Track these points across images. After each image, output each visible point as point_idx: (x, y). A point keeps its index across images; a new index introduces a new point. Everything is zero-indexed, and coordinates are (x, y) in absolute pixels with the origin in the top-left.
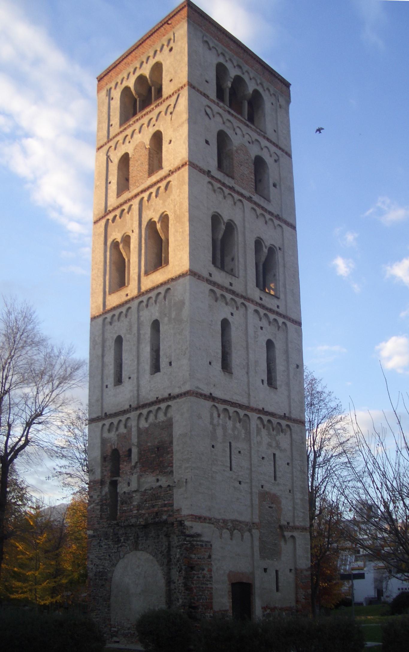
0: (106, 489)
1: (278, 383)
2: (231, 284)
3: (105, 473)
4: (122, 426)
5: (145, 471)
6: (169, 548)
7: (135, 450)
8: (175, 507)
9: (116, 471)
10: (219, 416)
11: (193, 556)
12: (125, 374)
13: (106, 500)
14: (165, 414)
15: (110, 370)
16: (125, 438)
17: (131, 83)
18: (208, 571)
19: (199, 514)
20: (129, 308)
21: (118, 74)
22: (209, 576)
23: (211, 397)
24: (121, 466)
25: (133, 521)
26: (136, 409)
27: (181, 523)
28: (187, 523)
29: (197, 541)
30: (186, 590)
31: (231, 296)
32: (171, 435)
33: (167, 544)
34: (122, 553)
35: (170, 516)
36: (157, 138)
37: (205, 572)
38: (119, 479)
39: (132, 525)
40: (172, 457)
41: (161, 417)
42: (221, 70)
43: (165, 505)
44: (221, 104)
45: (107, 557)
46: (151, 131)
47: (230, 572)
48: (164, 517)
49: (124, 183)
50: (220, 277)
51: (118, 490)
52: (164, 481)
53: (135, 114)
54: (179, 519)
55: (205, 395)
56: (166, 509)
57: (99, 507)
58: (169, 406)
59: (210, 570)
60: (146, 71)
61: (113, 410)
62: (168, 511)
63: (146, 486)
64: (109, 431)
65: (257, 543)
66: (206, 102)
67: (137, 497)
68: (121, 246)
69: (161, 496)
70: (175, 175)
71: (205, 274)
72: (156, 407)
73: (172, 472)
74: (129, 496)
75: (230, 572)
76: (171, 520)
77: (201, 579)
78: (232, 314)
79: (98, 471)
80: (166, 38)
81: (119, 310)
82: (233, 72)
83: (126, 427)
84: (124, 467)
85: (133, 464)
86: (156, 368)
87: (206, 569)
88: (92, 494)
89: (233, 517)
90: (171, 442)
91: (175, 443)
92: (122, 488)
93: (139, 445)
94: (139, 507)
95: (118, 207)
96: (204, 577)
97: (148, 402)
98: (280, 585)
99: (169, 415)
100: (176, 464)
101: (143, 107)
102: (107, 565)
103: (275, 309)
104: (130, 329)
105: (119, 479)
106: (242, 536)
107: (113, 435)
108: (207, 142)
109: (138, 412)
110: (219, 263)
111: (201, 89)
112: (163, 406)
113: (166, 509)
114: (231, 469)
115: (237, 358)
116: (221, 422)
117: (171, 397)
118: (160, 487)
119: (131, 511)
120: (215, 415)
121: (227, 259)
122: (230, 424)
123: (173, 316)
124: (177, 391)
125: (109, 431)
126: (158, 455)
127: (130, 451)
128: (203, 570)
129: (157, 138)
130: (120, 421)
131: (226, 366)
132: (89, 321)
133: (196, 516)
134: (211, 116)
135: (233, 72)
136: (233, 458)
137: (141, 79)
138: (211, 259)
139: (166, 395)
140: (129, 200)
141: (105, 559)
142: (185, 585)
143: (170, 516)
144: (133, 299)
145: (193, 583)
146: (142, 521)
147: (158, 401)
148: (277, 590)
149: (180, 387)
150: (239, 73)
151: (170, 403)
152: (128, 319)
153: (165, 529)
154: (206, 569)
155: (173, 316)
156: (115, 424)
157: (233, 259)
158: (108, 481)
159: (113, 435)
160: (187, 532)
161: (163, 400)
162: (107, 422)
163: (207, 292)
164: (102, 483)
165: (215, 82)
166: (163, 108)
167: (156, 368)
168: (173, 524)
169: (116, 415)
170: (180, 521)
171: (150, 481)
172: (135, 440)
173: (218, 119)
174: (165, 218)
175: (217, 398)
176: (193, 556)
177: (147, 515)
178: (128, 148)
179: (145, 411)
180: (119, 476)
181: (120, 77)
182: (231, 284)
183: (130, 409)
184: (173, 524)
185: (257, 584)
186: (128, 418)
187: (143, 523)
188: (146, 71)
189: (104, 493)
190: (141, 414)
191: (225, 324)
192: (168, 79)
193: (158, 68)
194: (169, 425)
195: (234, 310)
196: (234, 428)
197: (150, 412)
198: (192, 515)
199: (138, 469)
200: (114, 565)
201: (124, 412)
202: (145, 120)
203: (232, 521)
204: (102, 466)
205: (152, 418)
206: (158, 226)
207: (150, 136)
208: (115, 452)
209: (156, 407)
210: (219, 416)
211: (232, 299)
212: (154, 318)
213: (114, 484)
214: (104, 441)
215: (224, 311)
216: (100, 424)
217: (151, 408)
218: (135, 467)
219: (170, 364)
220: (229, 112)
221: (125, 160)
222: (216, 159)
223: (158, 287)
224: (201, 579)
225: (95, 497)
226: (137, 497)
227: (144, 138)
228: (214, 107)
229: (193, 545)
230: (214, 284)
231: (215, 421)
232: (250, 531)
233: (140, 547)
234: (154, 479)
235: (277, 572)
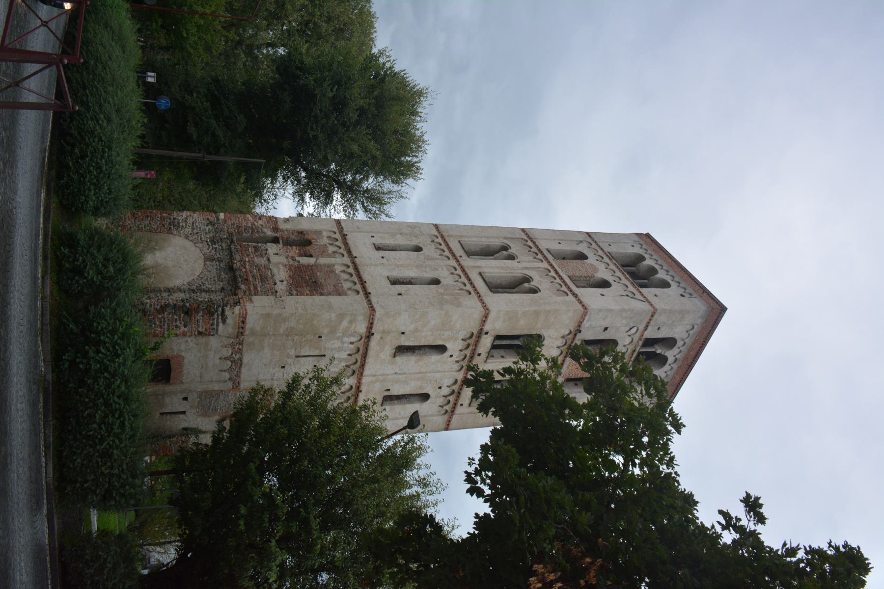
0: (269, 233)
1: (388, 408)
2: (479, 355)
3: (286, 233)
4: (335, 249)
5: (290, 269)
6: (208, 291)
7: (311, 261)
8: (255, 298)
9: (288, 243)
10: (352, 343)
11: (201, 314)
12: (386, 253)
13: (258, 232)
14: (349, 289)
15: (390, 241)
16: (323, 252)
17: (649, 262)
18: (184, 332)
19: (247, 320)
20: (449, 259)
21: (654, 250)
22: (178, 332)
23: (369, 335)
24: (294, 247)
25: (237, 257)
26: (354, 263)
27: (237, 303)
28: (237, 309)
29: (218, 318)
30: (161, 307)
31: (468, 355)
32: (330, 294)
33: (213, 289)
34: (200, 245)
35: (245, 292)
36: (605, 284)
37: (183, 328)
38: (281, 246)
39: (232, 256)
40: (307, 295)
41: (346, 285)
42: (670, 342)
43: (255, 288)
44: (641, 343)
45: (195, 231)
46: (610, 279)
47: (183, 358)
48: (243, 287)
49: (563, 257)
50: (486, 342)
51: (269, 244)
52: (281, 287)
53: (623, 266)
54: (241, 301)
55: (371, 328)
56: (252, 288)
57: (250, 225)
58: (358, 292)
59: (184, 334)
60: (662, 275)
61: (350, 242)
62: (250, 290)
63: (275, 271)
64: (329, 237)
65: (216, 387)
66: (641, 328)
67: (262, 261)
68: (504, 252)
69: (264, 283)
70: (574, 299)
71: (487, 328)
72: (356, 280)
73: (292, 295)
74: (265, 254)
75: (183, 358)
76: (240, 293)
77: (174, 324)
78: (451, 356)
79: (288, 226)
80: (692, 292)
81: (446, 249)
82: (670, 354)
83: (334, 252)
84: (294, 251)
85: (297, 258)
86: (395, 282)
87: (186, 329)
88: (264, 219)
89: (245, 360)
90: (322, 294)
91: (322, 297)
92: (272, 248)
93: (316, 265)
94: (252, 263)
95: (539, 250)
96: (177, 326)
97: (362, 273)
98: (168, 417)
99: (349, 292)
100: (301, 299)
101: (629, 273)
102: (187, 230)
103: (460, 402)
104: (429, 259)
105: (281, 246)
106: (225, 371)
107: (325, 241)
108: (606, 329)
109: (350, 264)
110: (498, 342)
111: (652, 323)
112: (358, 287)
113: (252, 288)
114: (297, 357)
115: (408, 362)
116: (346, 345)
117: (367, 295)
118: (275, 284)
119: (248, 255)
120: (353, 339)
121: (502, 352)
122: (344, 355)
123: (445, 297)
124: (374, 300)
125: (329, 237)
126: (306, 281)
127: (311, 256)
128: (185, 326)
129: (605, 284)
130: (340, 248)
131: (402, 350)
132: (434, 223)
133: (245, 318)
134: (629, 333)
135: (670, 354)
136: (309, 358)
137: (654, 271)
138: (501, 334)
139: (369, 290)
140: (547, 259)
141: (193, 229)
142: (167, 306)
143: (245, 292)
144: (458, 261)
145: (169, 314)
146: (237, 265)
147: (363, 283)
148: (162, 414)
149: (378, 302)
150: (671, 360)
151: (361, 293)
152: (438, 257)
153: (230, 288)
154: (186, 329)
155: (445, 297)
156: (337, 243)
157: (503, 357)
158: (278, 235)
159: (325, 241)
160: (227, 309)
161: (364, 288)
162: (338, 236)
163: (470, 330)
164: (276, 229)
165: (660, 336)
166: (631, 288)
167: (395, 282)
168: (236, 295)
169: (346, 244)
170: (239, 302)
171: (281, 274)
172: (322, 261)
173: (628, 340)
174: (534, 291)
175: (369, 341)
176: (201, 314)
177: (244, 270)
178: (592, 260)
179: (351, 270)
180: (284, 245)
181: (653, 253)
182: (479, 355)
183: (353, 258)
184: (236, 295)
185: (168, 388)
186: (343, 255)
187: (235, 266)
188: (662, 275)
189: (265, 230)
190: (348, 267)
191: (441, 349)
192: (657, 293)
193: (665, 285)
194: (339, 292)
195: (454, 358)
196: (341, 360)
197: (351, 275)
198: (246, 313)
199: (292, 262)
200: (187, 237)
201: (349, 252)
202: (618, 274)
203: (241, 359)
204: (293, 232)
205: (345, 276)
206: (526, 285)
207: (606, 278)
208: (309, 243)
209: (356, 280)
210: (352, 343)
211: (466, 356)
212: (442, 280)
213: (275, 240)
214: (319, 233)
215: (454, 347)
216: (335, 229)
217: (354, 276)
218: (294, 260)
219: (400, 294)
220: (634, 351)
221: (582, 257)
222: (592, 338)
223: (471, 284)
224: (174, 324)
225: (260, 222)
226: (262, 261)
227: (603, 273)
228: (638, 335)
229: (213, 314)
230: (479, 336)
231: (346, 339)
232: (230, 379)
233: (208, 263)
234: (283, 278)
235: (184, 413)
